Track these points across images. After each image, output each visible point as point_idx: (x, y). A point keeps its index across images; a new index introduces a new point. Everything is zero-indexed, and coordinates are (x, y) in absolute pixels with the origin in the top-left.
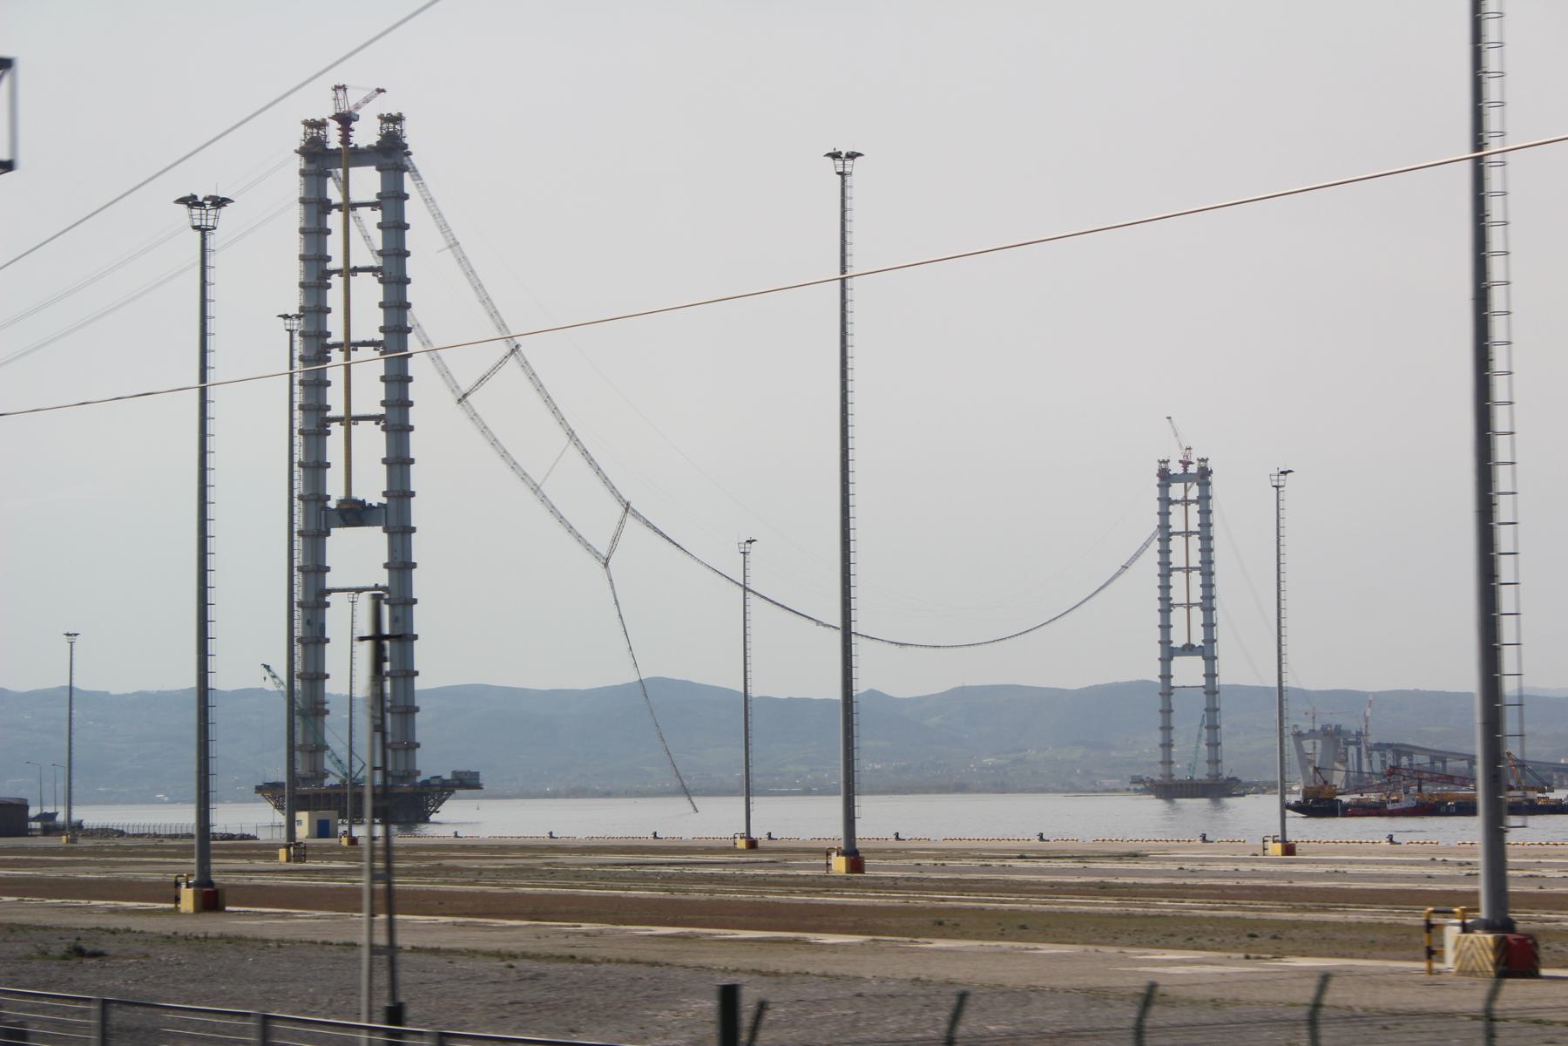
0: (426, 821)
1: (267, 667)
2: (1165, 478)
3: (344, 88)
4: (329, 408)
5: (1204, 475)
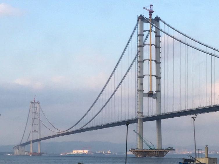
1: (134, 131)
3: (152, 5)
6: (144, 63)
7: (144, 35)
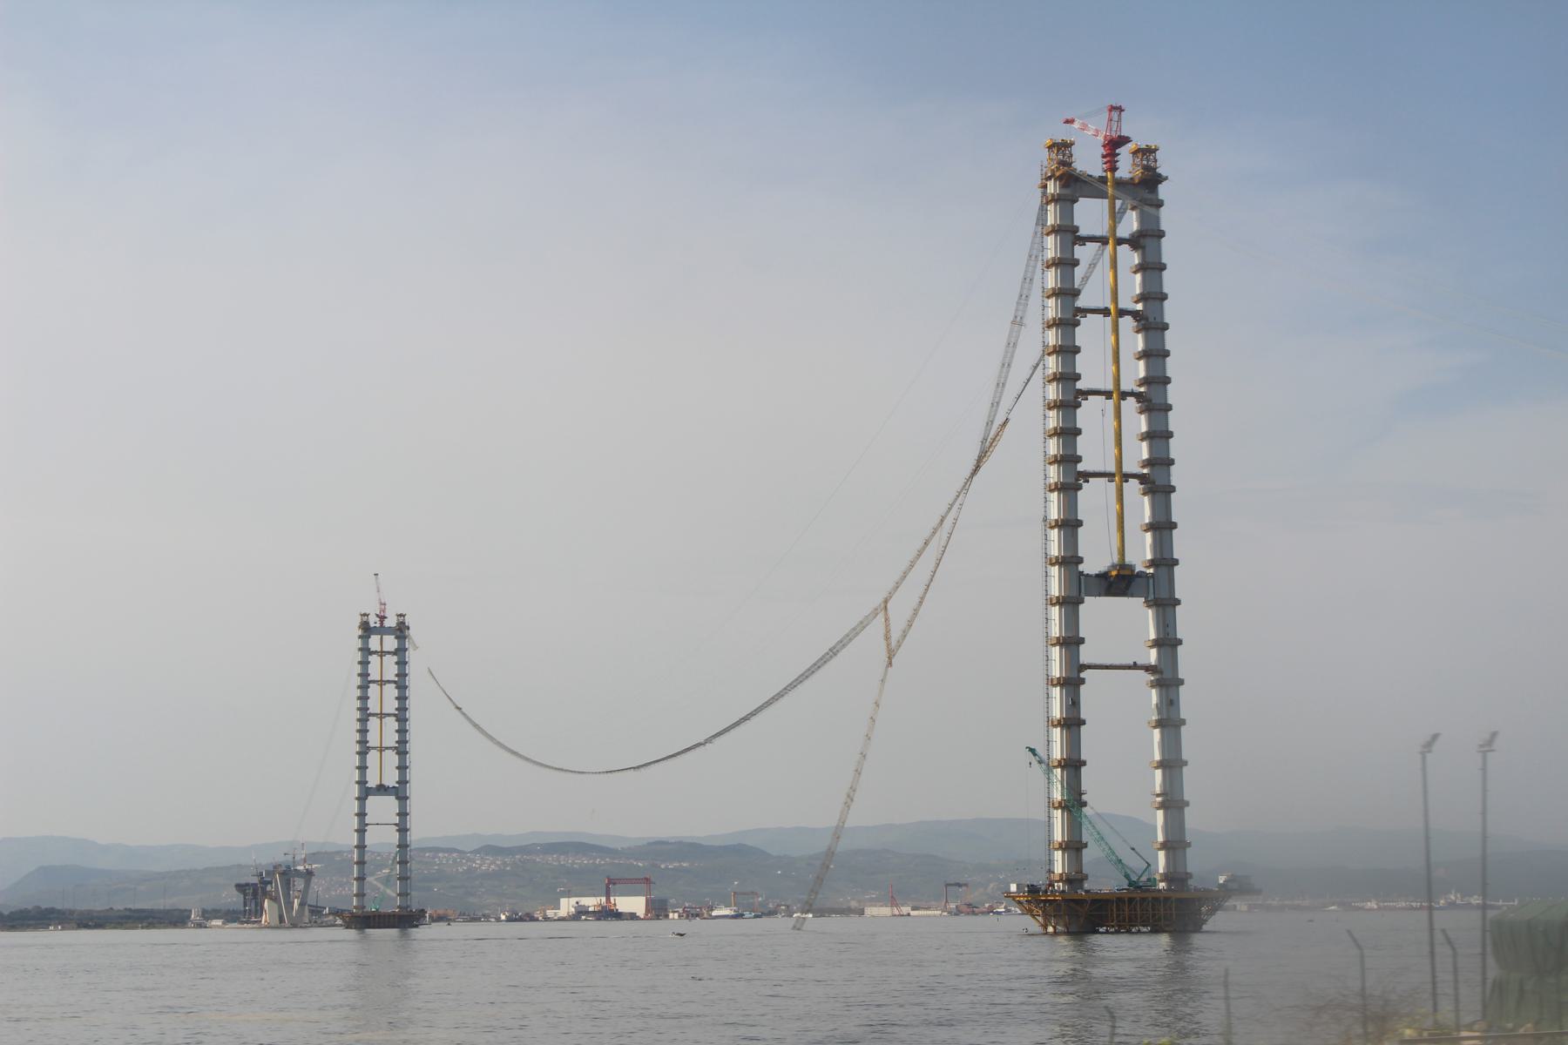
0: (1198, 929)
1: (1032, 751)
2: (366, 630)
3: (1120, 109)
4: (1079, 459)
5: (401, 631)
6: (1080, 493)
7: (1076, 263)
